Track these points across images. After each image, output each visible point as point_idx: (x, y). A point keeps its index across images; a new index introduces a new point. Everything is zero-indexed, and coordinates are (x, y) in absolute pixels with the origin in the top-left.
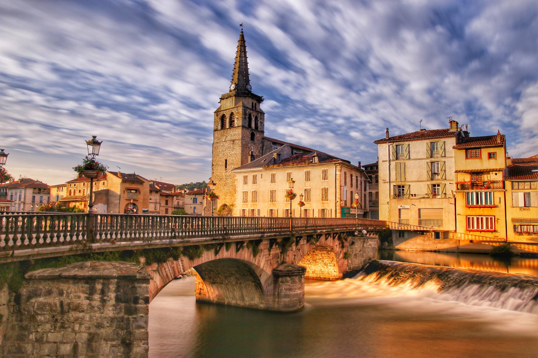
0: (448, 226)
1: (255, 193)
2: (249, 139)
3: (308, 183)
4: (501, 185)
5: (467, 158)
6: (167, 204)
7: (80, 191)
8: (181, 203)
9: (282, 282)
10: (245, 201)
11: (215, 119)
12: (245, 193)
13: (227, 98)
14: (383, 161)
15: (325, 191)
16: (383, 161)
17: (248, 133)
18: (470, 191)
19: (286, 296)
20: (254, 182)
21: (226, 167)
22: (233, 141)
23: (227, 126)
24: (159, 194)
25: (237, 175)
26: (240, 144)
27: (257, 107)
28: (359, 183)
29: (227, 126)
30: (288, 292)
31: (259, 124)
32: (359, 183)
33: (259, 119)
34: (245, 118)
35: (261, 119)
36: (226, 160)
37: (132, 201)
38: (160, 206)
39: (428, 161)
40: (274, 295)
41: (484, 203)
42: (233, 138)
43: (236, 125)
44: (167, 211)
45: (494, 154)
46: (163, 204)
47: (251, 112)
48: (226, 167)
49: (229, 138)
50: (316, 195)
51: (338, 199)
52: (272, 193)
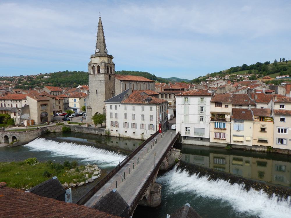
0: (206, 136)
1: (116, 114)
2: (108, 80)
3: (125, 111)
4: (229, 120)
5: (215, 107)
6: (59, 103)
7: (9, 105)
8: (66, 101)
9: (154, 195)
10: (111, 117)
11: (89, 68)
12: (111, 114)
13: (95, 57)
14: (179, 104)
15: (151, 117)
16: (179, 104)
17: (108, 76)
18: (217, 122)
19: (155, 200)
20: (6, 138)
21: (97, 94)
22: (100, 81)
23: (96, 72)
24: (54, 99)
25: (106, 104)
26: (104, 83)
27: (111, 61)
28: (165, 107)
29: (96, 72)
30: (156, 199)
31: (112, 70)
32: (165, 107)
33: (112, 68)
34: (106, 69)
35: (113, 68)
36: (97, 90)
37: (44, 111)
38: (56, 105)
39: (199, 106)
40: (150, 200)
41: (222, 127)
42: (100, 79)
43: (101, 73)
44: (60, 108)
45: (227, 106)
46: (57, 104)
47: (109, 65)
48: (97, 94)
49: (97, 79)
50: (147, 118)
51: (157, 121)
52: (126, 115)
